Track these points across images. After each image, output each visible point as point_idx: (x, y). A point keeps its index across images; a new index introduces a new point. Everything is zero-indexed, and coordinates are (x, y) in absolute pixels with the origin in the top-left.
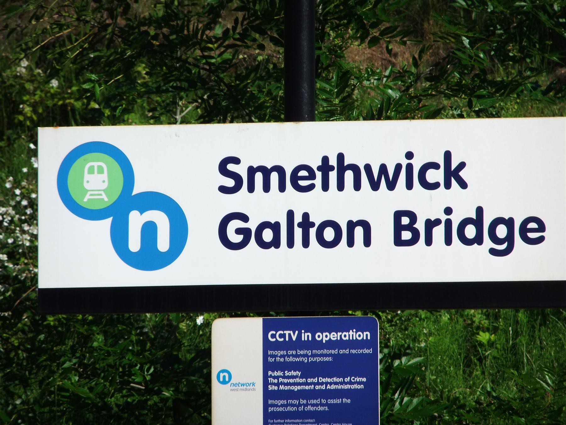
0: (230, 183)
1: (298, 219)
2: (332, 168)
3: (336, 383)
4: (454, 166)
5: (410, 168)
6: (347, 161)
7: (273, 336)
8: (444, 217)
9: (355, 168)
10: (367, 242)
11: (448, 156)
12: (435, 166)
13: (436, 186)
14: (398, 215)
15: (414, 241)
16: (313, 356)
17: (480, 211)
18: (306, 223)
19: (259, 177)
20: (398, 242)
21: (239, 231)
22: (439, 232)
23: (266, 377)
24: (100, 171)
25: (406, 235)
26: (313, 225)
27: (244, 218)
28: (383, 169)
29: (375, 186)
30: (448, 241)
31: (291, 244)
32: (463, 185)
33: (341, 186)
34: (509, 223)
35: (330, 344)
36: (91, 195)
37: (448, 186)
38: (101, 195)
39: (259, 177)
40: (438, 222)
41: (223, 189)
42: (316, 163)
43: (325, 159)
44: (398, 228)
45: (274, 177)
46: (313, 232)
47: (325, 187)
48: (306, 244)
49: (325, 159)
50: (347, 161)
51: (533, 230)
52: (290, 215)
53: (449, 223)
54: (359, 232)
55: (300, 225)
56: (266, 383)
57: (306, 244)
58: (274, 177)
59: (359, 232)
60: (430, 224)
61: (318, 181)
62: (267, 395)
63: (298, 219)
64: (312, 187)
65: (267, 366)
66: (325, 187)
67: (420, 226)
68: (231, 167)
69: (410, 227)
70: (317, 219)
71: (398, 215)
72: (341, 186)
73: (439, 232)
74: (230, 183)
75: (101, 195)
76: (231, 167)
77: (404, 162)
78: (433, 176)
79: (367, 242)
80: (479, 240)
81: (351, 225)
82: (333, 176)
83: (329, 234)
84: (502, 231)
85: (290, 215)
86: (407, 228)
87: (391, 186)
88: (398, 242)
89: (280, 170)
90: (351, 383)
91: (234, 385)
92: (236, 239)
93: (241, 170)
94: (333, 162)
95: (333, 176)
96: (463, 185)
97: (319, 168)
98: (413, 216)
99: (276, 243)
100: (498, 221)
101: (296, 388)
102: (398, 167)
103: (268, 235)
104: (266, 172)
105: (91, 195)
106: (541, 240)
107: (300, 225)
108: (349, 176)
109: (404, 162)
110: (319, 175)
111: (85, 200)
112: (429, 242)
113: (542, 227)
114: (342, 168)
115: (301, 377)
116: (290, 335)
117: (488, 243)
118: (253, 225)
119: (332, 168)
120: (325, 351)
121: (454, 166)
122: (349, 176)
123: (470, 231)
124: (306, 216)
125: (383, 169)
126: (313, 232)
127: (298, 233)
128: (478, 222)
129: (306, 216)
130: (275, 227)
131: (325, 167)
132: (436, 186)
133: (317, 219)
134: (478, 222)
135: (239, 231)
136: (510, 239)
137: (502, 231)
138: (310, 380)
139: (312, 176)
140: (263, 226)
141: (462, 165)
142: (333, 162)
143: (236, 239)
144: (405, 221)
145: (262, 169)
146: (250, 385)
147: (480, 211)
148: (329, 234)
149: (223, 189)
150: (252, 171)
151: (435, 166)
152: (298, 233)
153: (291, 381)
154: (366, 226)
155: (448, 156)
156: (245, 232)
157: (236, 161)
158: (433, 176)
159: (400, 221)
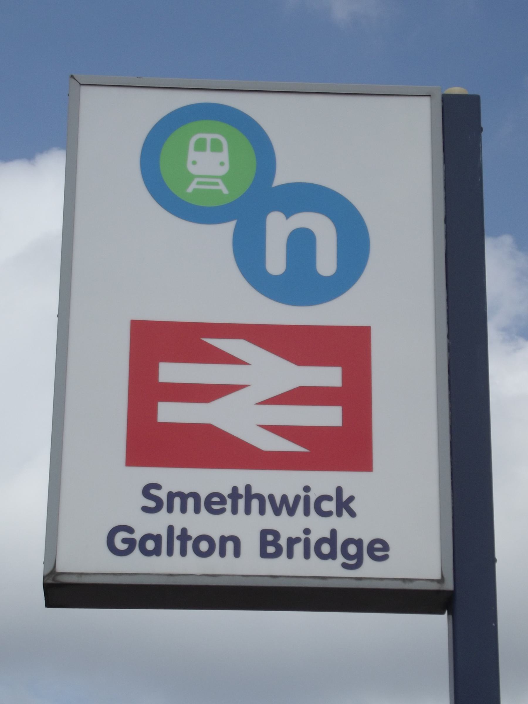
0: (152, 504)
1: (177, 532)
2: (241, 496)
4: (345, 497)
5: (307, 499)
6: (254, 491)
8: (303, 536)
9: (260, 498)
11: (339, 490)
12: (328, 498)
13: (328, 514)
14: (264, 533)
15: (277, 554)
18: (184, 536)
19: (177, 501)
20: (264, 554)
21: (124, 541)
22: (299, 548)
24: (216, 147)
25: (271, 549)
26: (190, 538)
27: (130, 530)
28: (284, 498)
30: (307, 555)
31: (170, 552)
32: (352, 514)
33: (248, 511)
34: (359, 543)
37: (339, 514)
38: (217, 184)
39: (177, 501)
40: (298, 540)
41: (145, 509)
42: (226, 491)
43: (235, 489)
44: (264, 544)
45: (191, 502)
46: (190, 544)
47: (235, 511)
48: (183, 553)
49: (235, 489)
50: (254, 491)
51: (379, 550)
52: (171, 529)
53: (307, 542)
54: (230, 545)
55: (178, 538)
57: (183, 553)
58: (191, 502)
59: (230, 545)
60: (291, 542)
63: (177, 532)
64: (223, 511)
66: (235, 511)
67: (283, 542)
68: (153, 492)
69: (275, 543)
70: (193, 533)
71: (264, 533)
72: (248, 511)
73: (299, 548)
74: (152, 504)
75: (217, 184)
76: (153, 492)
77: (302, 494)
78: (326, 506)
80: (332, 555)
81: (224, 540)
82: (241, 503)
83: (204, 546)
84: (352, 549)
85: (171, 529)
86: (271, 543)
87: (291, 512)
88: (264, 554)
89: (195, 496)
92: (123, 547)
93: (162, 494)
94: (242, 491)
95: (241, 503)
96: (352, 514)
97: (229, 496)
98: (276, 534)
99: (157, 551)
102: (297, 498)
103: (150, 545)
104: (184, 497)
106: (385, 558)
107: (178, 538)
108: (255, 503)
109: (302, 494)
110: (229, 501)
112: (290, 555)
113: (386, 547)
117: (340, 559)
118: (137, 536)
119: (241, 496)
121: (345, 497)
122: (255, 503)
123: (326, 549)
124: (184, 531)
125: (284, 498)
126: (190, 544)
127: (177, 544)
130: (157, 539)
132: (328, 514)
133: (193, 533)
135: (124, 541)
136: (359, 556)
137: (352, 549)
139: (223, 501)
140: (147, 537)
141: (351, 499)
142: (242, 491)
143: (123, 547)
144: (270, 538)
145: (180, 494)
147: (334, 532)
148: (204, 546)
149: (145, 509)
150: (171, 496)
151: (328, 498)
152: (177, 544)
154: (236, 540)
155: (339, 490)
156: (131, 543)
157: (158, 487)
158: (326, 506)
159: (266, 537)
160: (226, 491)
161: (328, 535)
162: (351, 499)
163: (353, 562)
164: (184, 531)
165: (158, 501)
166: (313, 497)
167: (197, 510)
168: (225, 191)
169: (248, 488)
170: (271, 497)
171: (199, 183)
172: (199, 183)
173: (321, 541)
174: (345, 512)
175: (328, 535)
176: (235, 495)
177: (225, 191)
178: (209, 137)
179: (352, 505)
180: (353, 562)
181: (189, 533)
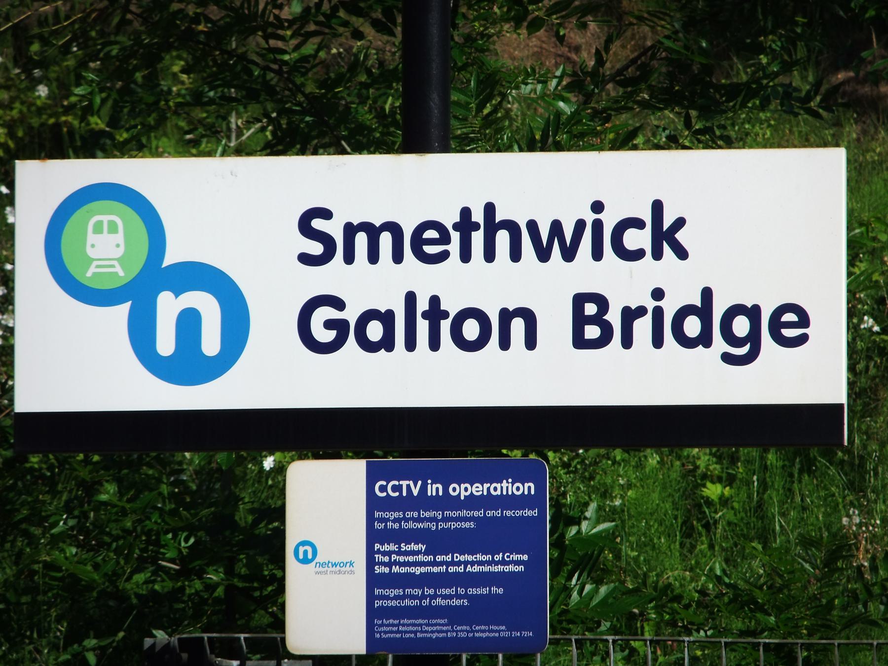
0: (316, 248)
1: (422, 305)
2: (476, 227)
3: (481, 563)
4: (667, 223)
5: (598, 226)
7: (383, 489)
8: (650, 304)
9: (512, 227)
10: (531, 342)
11: (657, 207)
12: (638, 224)
13: (638, 255)
14: (579, 300)
16: (445, 520)
17: (707, 294)
18: (435, 313)
19: (361, 240)
20: (580, 342)
21: (329, 324)
22: (643, 327)
23: (370, 553)
24: (113, 228)
25: (592, 332)
26: (446, 314)
27: (338, 304)
28: (556, 227)
29: (543, 255)
31: (411, 345)
32: (682, 253)
33: (490, 255)
34: (753, 313)
35: (472, 502)
36: (97, 267)
37: (657, 255)
39: (361, 240)
40: (641, 311)
41: (306, 259)
42: (450, 219)
43: (466, 213)
44: (580, 320)
45: (386, 240)
46: (445, 326)
47: (466, 256)
48: (435, 345)
49: (466, 213)
52: (411, 299)
53: (658, 313)
54: (518, 326)
55: (425, 315)
56: (371, 563)
58: (386, 240)
59: (518, 326)
60: (630, 315)
61: (454, 247)
62: (373, 581)
63: (422, 305)
64: (443, 256)
65: (374, 536)
66: (466, 256)
67: (614, 317)
68: (318, 224)
69: (598, 320)
70: (452, 306)
71: (579, 300)
72: (490, 255)
73: (643, 327)
74: (316, 248)
76: (318, 224)
78: (634, 239)
79: (531, 342)
80: (705, 339)
81: (506, 316)
82: (478, 238)
83: (471, 329)
85: (411, 299)
87: (569, 254)
88: (580, 342)
89: (394, 229)
90: (503, 563)
91: (322, 565)
92: (325, 336)
93: (334, 228)
94: (478, 216)
95: (478, 238)
96: (682, 253)
97: (456, 227)
98: (602, 302)
99: (387, 343)
100: (735, 311)
101: (418, 571)
102: (580, 225)
103: (375, 330)
104: (373, 232)
105: (97, 267)
106: (802, 340)
107: (425, 315)
108: (503, 238)
109: (590, 217)
110: (455, 236)
111: (89, 274)
112: (627, 342)
113: (804, 320)
114: (492, 226)
115: (426, 553)
116: (408, 486)
117: (719, 345)
118: (351, 315)
119: (476, 227)
120: (464, 513)
121: (667, 223)
122: (503, 238)
123: (692, 326)
124: (435, 301)
125: (556, 227)
126: (445, 326)
127: (423, 327)
128: (704, 311)
129: (435, 301)
130: (387, 318)
131: (465, 224)
132: (638, 255)
133: (452, 306)
134: (704, 311)
135: (329, 324)
136: (754, 338)
137: (741, 326)
138: (439, 558)
139: (445, 238)
141: (680, 223)
142: (478, 216)
143: (325, 336)
145: (367, 227)
146: (342, 566)
147: (707, 294)
148: (471, 329)
149: (306, 259)
150: (350, 230)
151: (638, 224)
152: (423, 327)
153: (411, 559)
154: (528, 316)
155: (657, 207)
156: (340, 326)
157: (326, 214)
158: (634, 239)
159: (583, 309)
161: (698, 302)
162: (680, 223)
166: (609, 223)
168: (121, 274)
174: (666, 248)
175: (698, 302)
177: (121, 274)
179: (681, 236)
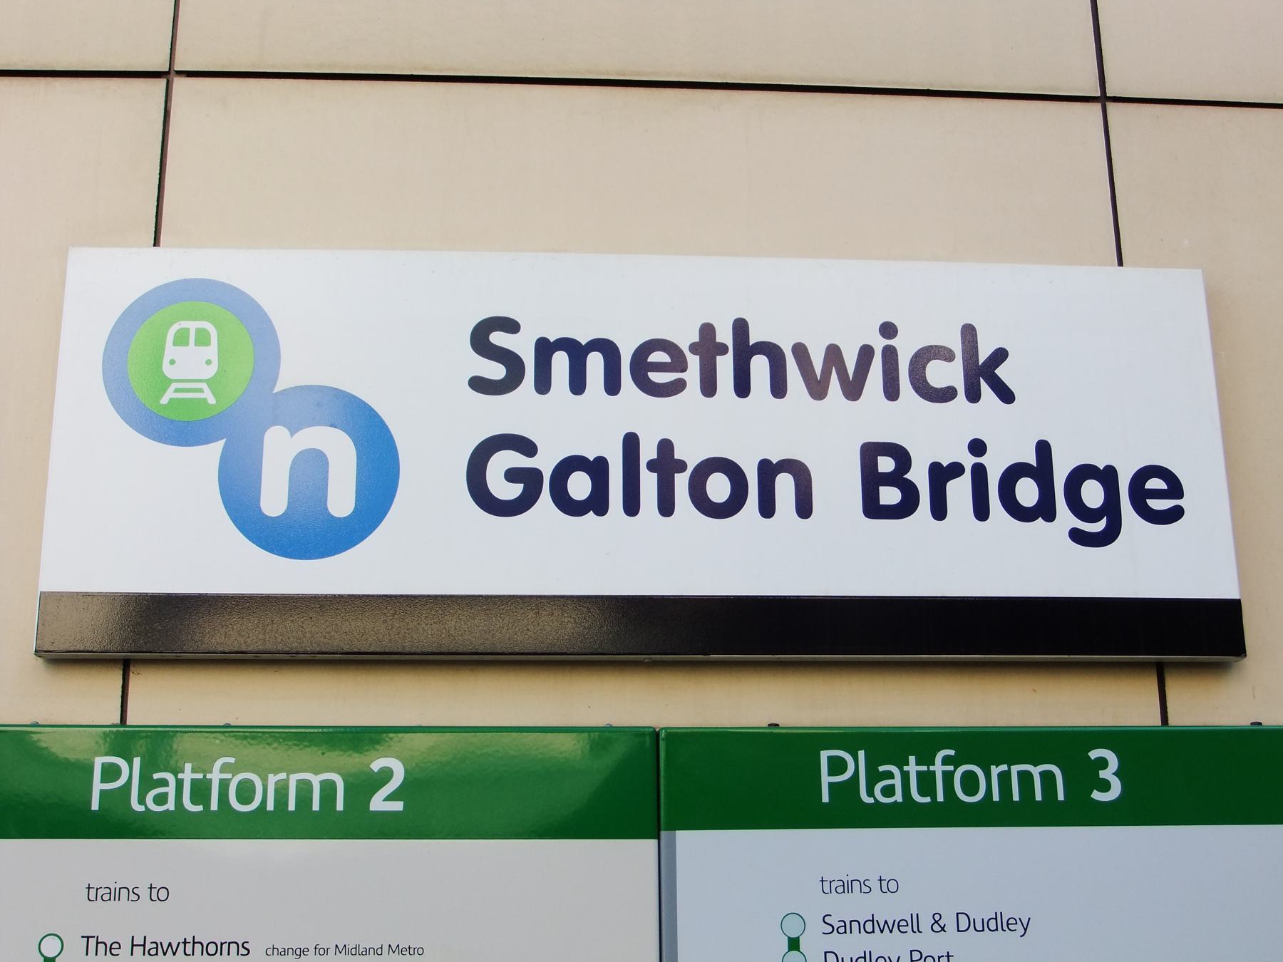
0: (496, 371)
1: (648, 452)
2: (723, 349)
4: (984, 354)
5: (890, 355)
8: (968, 461)
9: (772, 352)
11: (969, 333)
12: (944, 354)
13: (946, 395)
14: (871, 452)
15: (906, 507)
18: (666, 463)
19: (561, 362)
20: (873, 509)
21: (512, 475)
22: (959, 491)
25: (890, 495)
26: (682, 466)
27: (527, 447)
28: (834, 354)
31: (632, 506)
32: (1006, 395)
33: (742, 387)
34: (1108, 477)
37: (973, 396)
39: (561, 362)
41: (480, 385)
42: (686, 337)
43: (707, 331)
44: (872, 481)
45: (595, 363)
46: (682, 482)
47: (709, 387)
49: (707, 331)
52: (631, 443)
53: (979, 474)
54: (785, 485)
55: (652, 466)
57: (666, 507)
58: (595, 363)
59: (785, 485)
60: (941, 475)
63: (648, 452)
64: (678, 387)
66: (709, 387)
67: (919, 476)
69: (898, 478)
70: (691, 453)
71: (871, 452)
72: (742, 387)
73: (959, 491)
74: (496, 371)
80: (1045, 510)
81: (768, 471)
84: (1093, 494)
85: (631, 443)
86: (891, 479)
87: (853, 390)
89: (608, 349)
92: (510, 491)
94: (725, 336)
95: (725, 366)
96: (1006, 395)
97: (694, 348)
98: (902, 457)
99: (598, 504)
104: (578, 353)
106: (1175, 515)
107: (652, 466)
108: (760, 367)
109: (879, 343)
110: (694, 362)
112: (939, 511)
113: (1175, 489)
117: (1066, 518)
118: (545, 463)
119: (723, 349)
122: (760, 367)
123: (1027, 492)
124: (666, 447)
125: (834, 354)
126: (682, 482)
127: (649, 483)
130: (597, 469)
132: (946, 395)
133: (691, 453)
135: (512, 475)
136: (1111, 508)
139: (679, 363)
141: (1000, 356)
142: (725, 336)
145: (567, 344)
148: (718, 488)
149: (480, 385)
150: (545, 349)
151: (944, 354)
152: (649, 483)
155: (969, 333)
156: (530, 479)
157: (511, 326)
160: (686, 337)
162: (1000, 356)
163: (1099, 526)
164: (666, 447)
165: (511, 361)
167: (612, 386)
169: (741, 328)
170: (801, 352)
171: (177, 390)
172: (177, 390)
173: (1013, 474)
176: (707, 345)
178: (192, 326)
180: (1099, 526)
181: (678, 455)
